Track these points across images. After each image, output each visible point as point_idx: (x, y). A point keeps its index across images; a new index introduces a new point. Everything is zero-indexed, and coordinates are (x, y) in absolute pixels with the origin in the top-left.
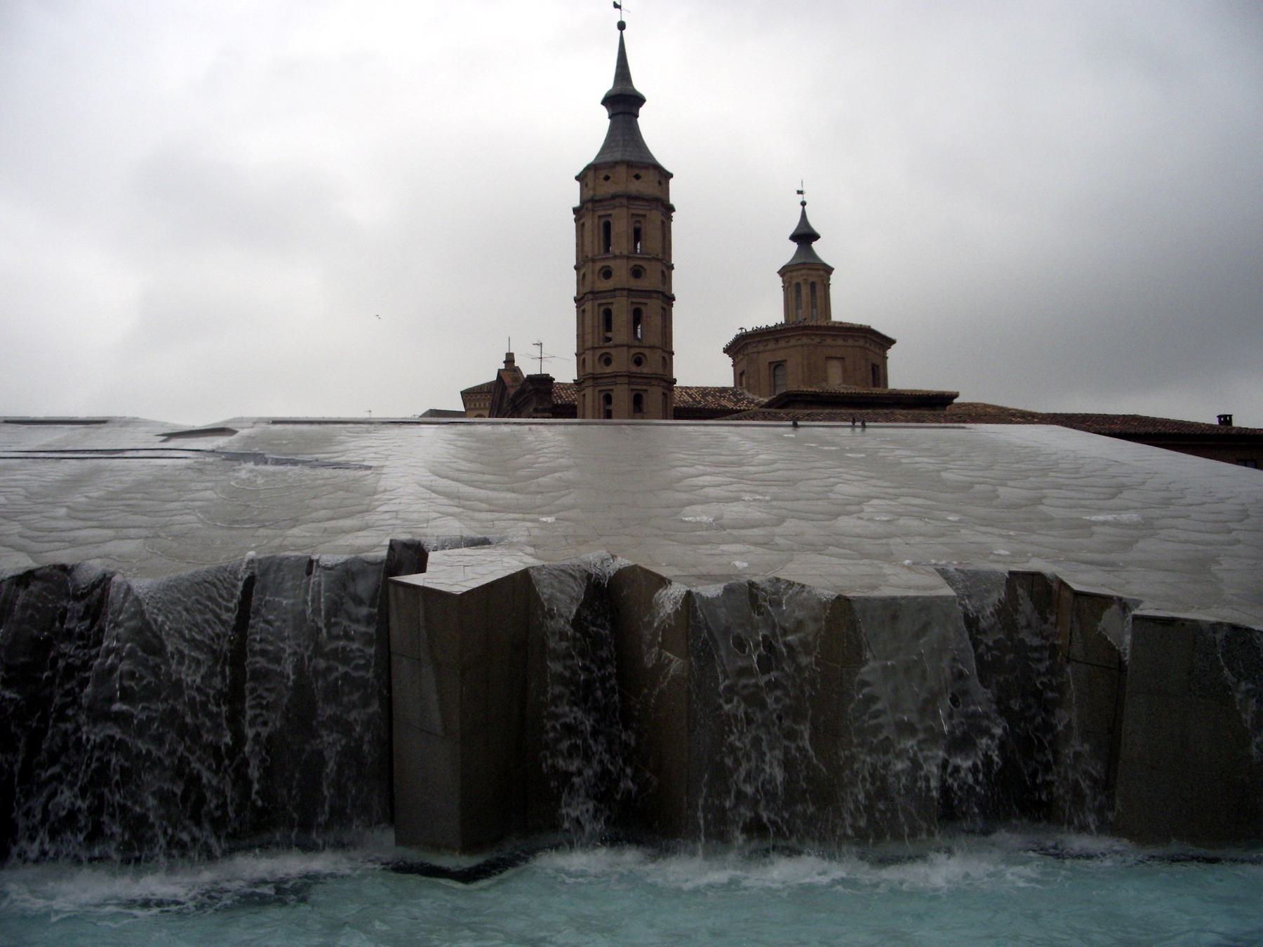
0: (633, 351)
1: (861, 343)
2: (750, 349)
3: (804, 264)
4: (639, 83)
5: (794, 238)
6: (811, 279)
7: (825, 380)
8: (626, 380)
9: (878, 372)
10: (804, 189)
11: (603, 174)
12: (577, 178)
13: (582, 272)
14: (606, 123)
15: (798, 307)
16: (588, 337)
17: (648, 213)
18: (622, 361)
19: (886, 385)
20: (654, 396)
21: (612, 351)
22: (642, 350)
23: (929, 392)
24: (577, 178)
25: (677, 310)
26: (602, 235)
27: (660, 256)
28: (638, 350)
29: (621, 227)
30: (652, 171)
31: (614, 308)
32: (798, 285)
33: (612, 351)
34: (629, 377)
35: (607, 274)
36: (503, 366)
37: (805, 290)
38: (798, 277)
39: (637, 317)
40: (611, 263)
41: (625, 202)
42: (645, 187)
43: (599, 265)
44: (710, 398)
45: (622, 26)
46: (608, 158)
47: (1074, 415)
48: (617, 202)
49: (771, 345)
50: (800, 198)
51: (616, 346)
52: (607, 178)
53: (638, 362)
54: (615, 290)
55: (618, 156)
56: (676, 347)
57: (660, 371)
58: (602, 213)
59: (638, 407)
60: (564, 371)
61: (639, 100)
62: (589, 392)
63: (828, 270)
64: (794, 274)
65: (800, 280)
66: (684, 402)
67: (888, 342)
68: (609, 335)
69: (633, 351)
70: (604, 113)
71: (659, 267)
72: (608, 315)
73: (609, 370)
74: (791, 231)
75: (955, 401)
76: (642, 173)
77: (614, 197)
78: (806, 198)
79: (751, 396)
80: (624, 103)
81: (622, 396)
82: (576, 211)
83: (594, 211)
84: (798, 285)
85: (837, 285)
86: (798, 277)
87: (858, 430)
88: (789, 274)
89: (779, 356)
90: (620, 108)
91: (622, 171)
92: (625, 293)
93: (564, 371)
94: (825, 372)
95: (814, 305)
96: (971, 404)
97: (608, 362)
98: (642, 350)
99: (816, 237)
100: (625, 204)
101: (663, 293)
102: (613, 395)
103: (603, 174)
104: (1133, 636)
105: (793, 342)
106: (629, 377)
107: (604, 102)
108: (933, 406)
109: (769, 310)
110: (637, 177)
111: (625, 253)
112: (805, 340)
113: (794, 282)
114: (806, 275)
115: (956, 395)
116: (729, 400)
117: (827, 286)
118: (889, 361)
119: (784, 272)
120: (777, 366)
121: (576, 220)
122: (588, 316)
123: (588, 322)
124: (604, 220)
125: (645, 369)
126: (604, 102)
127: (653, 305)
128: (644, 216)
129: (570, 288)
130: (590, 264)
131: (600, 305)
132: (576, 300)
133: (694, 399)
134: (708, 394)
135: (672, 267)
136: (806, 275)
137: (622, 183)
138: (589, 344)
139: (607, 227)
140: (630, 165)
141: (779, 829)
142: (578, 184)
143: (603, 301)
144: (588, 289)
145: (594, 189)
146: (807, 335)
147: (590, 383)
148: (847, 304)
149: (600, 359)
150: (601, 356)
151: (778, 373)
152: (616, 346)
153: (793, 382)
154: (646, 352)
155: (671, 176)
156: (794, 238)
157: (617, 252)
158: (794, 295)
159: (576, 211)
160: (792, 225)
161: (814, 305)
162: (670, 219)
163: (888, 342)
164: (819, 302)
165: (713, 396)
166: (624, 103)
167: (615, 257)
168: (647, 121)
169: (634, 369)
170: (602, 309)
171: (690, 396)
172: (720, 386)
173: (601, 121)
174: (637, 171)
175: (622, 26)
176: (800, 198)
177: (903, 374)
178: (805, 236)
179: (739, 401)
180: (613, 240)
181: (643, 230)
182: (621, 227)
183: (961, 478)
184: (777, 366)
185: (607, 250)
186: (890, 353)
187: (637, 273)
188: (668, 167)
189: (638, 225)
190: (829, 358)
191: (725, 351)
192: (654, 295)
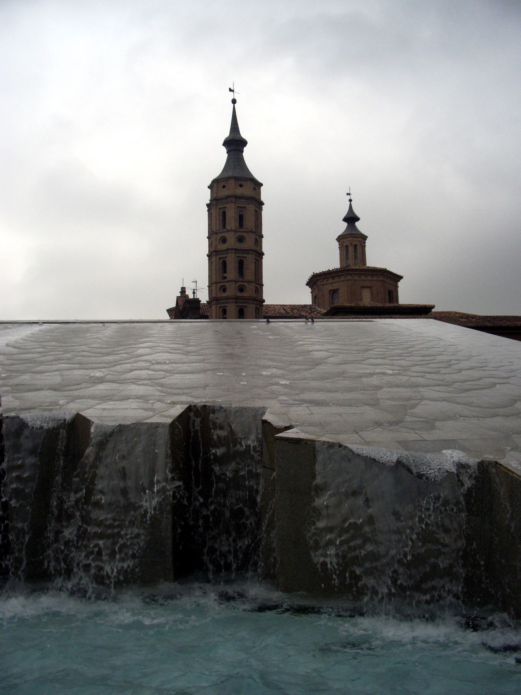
0: (238, 284)
1: (382, 278)
2: (319, 283)
3: (350, 234)
4: (244, 134)
5: (345, 220)
6: (354, 243)
7: (361, 300)
8: (234, 301)
9: (393, 295)
10: (351, 192)
11: (222, 184)
12: (209, 187)
13: (211, 240)
14: (226, 156)
15: (347, 259)
16: (214, 276)
17: (247, 206)
18: (232, 290)
19: (397, 301)
20: (251, 308)
21: (227, 284)
22: (243, 284)
23: (417, 305)
24: (209, 187)
25: (265, 260)
26: (221, 218)
27: (254, 230)
28: (241, 284)
29: (231, 214)
30: (249, 182)
31: (228, 260)
32: (347, 246)
33: (227, 284)
34: (236, 299)
36: (179, 295)
37: (351, 249)
38: (347, 242)
39: (241, 264)
41: (233, 200)
42: (247, 191)
43: (219, 236)
44: (296, 311)
45: (234, 101)
46: (225, 175)
47: (498, 317)
48: (229, 200)
49: (331, 281)
50: (348, 197)
51: (229, 281)
52: (224, 187)
53: (241, 290)
54: (228, 250)
55: (230, 174)
56: (265, 281)
57: (254, 295)
58: (221, 206)
59: (241, 314)
60: (204, 297)
61: (244, 143)
62: (214, 307)
63: (365, 238)
64: (345, 240)
65: (348, 244)
66: (280, 313)
67: (399, 278)
68: (225, 275)
69: (238, 284)
70: (224, 150)
71: (253, 236)
72: (224, 264)
73: (224, 295)
75: (433, 310)
76: (243, 183)
77: (227, 197)
78: (352, 197)
79: (319, 310)
80: (235, 144)
81: (232, 308)
82: (208, 205)
83: (216, 205)
84: (347, 246)
86: (347, 242)
87: (309, 323)
88: (341, 241)
89: (335, 286)
90: (232, 148)
91: (232, 182)
92: (234, 251)
93: (204, 297)
94: (361, 295)
95: (356, 258)
96: (448, 312)
97: (224, 290)
98: (243, 284)
99: (358, 219)
100: (235, 202)
101: (256, 251)
102: (227, 309)
103: (222, 184)
104: (90, 431)
105: (342, 278)
106: (236, 299)
107: (224, 145)
108: (421, 311)
109: (331, 260)
110: (241, 186)
111: (234, 228)
112: (349, 277)
113: (345, 244)
114: (352, 241)
115: (433, 307)
116: (307, 312)
117: (364, 247)
119: (340, 239)
120: (334, 292)
121: (208, 211)
122: (214, 264)
123: (214, 268)
124: (222, 210)
125: (245, 294)
126: (224, 145)
127: (250, 259)
128: (245, 207)
129: (205, 248)
130: (215, 235)
131: (220, 258)
132: (208, 256)
133: (286, 312)
134: (295, 309)
135: (262, 236)
136: (352, 241)
137: (232, 189)
138: (214, 280)
139: (224, 214)
140: (236, 179)
141: (78, 564)
142: (209, 190)
143: (221, 256)
144: (213, 250)
145: (217, 193)
146: (350, 274)
147: (214, 302)
148: (375, 257)
149: (220, 288)
150: (221, 286)
151: (334, 296)
152: (229, 281)
153: (342, 301)
154: (246, 284)
155: (262, 185)
156: (345, 220)
157: (229, 228)
158: (345, 252)
159: (208, 205)
160: (344, 213)
161: (356, 258)
162: (261, 209)
163: (399, 278)
164: (359, 256)
165: (298, 310)
166: (235, 144)
167: (228, 231)
168: (248, 154)
169: (239, 294)
170: (221, 260)
171: (285, 310)
172: (303, 304)
173: (222, 156)
174: (240, 183)
175: (234, 101)
176: (348, 197)
177: (406, 296)
178: (351, 219)
179: (312, 312)
180: (227, 221)
181: (244, 217)
182: (231, 214)
184: (334, 292)
185: (224, 226)
186: (400, 284)
187: (241, 240)
188: (260, 181)
189: (241, 213)
190: (363, 287)
191: (307, 284)
192: (250, 252)
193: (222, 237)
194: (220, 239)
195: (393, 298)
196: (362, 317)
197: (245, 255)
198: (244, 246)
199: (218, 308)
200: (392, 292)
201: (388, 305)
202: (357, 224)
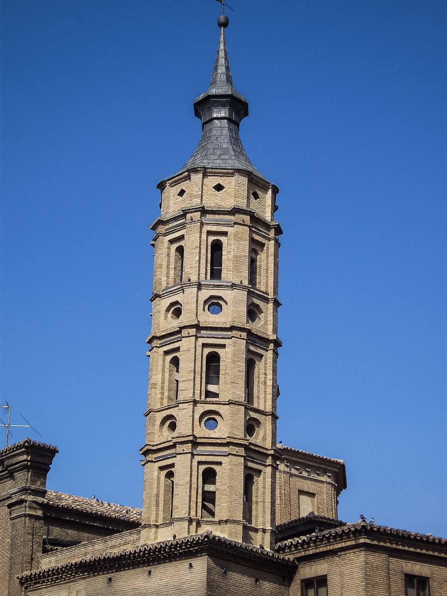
52: (219, 188)
68: (212, 388)
193: (212, 297)
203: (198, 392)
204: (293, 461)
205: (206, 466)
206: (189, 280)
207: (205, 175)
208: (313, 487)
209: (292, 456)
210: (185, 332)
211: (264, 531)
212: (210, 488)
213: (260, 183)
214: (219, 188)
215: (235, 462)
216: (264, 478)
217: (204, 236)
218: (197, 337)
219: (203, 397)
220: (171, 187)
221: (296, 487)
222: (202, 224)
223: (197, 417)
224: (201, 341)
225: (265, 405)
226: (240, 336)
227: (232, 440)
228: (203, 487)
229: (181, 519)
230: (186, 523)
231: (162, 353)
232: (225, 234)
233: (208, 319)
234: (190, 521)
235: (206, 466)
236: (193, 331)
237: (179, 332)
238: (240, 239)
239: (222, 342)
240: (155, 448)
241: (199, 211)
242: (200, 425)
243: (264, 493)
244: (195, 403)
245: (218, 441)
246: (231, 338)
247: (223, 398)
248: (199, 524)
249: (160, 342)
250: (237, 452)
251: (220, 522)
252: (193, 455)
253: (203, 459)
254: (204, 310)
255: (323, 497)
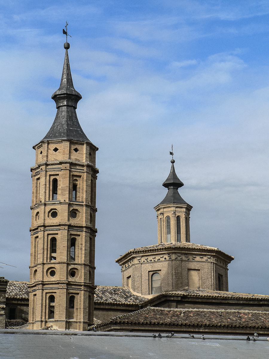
5: (166, 185)
6: (178, 214)
21: (56, 266)
33: (56, 266)
35: (54, 214)
40: (57, 207)
43: (48, 208)
52: (56, 150)
68: (54, 255)
74: (55, 89)
85: (196, 220)
89: (157, 266)
98: (76, 266)
99: (181, 185)
118: (229, 272)
124: (52, 178)
139: (55, 182)
155: (98, 149)
160: (165, 176)
175: (173, 162)
179: (127, 297)
183: (82, 315)
186: (229, 266)
187: (73, 214)
193: (52, 209)
194: (49, 212)
195: (222, 284)
196: (70, 243)
197: (79, 233)
198: (74, 222)
199: (44, 294)
200: (222, 276)
201: (216, 294)
202: (180, 190)
203: (45, 259)
204: (183, 253)
205: (50, 294)
206: (41, 202)
207: (48, 144)
208: (198, 266)
209: (182, 251)
210: (39, 230)
211: (80, 322)
212: (52, 304)
213: (78, 143)
214: (56, 150)
215: (62, 292)
216: (80, 297)
217: (48, 177)
218: (44, 231)
219: (49, 260)
220: (39, 149)
221: (186, 268)
222: (46, 171)
223: (45, 271)
224: (46, 233)
225: (81, 261)
226: (64, 228)
227: (59, 282)
228: (49, 304)
229: (38, 321)
230: (40, 323)
231: (34, 238)
232: (58, 175)
233: (51, 221)
234: (42, 321)
235: (50, 294)
236: (42, 228)
237: (37, 229)
238: (65, 178)
239: (56, 232)
240: (31, 286)
241: (45, 165)
242: (47, 276)
243: (80, 304)
244: (44, 264)
245: (54, 282)
246: (60, 230)
247: (58, 260)
248: (46, 322)
249: (34, 232)
250: (63, 287)
251: (55, 321)
252: (43, 290)
253: (47, 291)
254: (48, 216)
255: (205, 271)
